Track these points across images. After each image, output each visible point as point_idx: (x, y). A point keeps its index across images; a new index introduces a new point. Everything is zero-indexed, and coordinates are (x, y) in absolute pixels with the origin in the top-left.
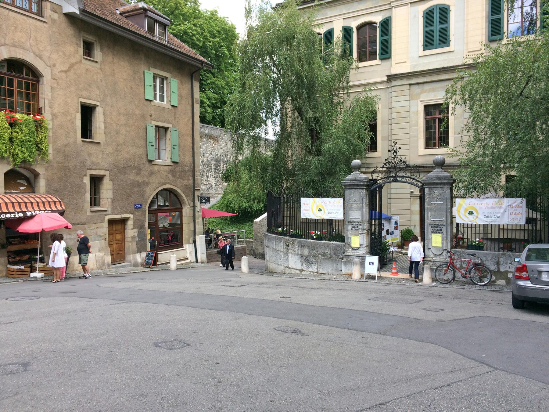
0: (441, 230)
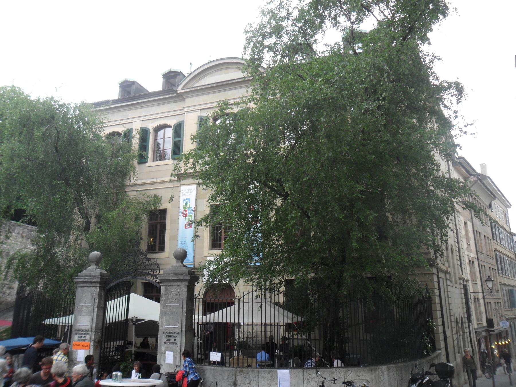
0: (175, 340)
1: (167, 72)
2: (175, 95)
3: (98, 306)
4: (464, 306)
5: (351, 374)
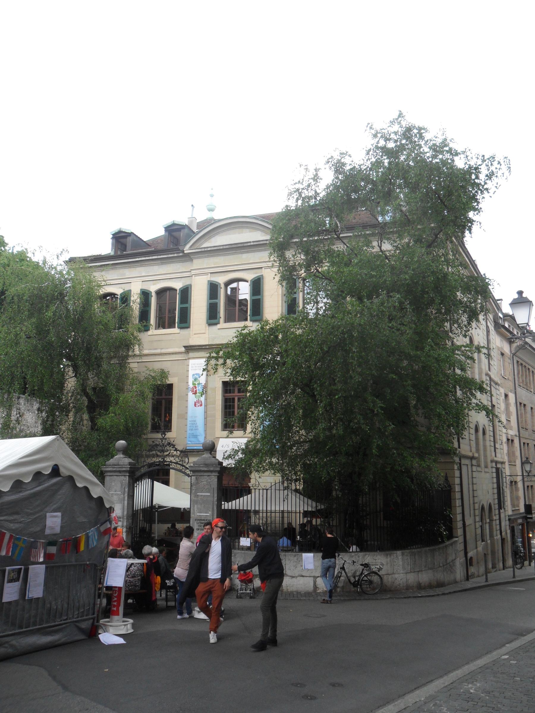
1: (169, 224)
2: (181, 254)
3: (128, 494)
4: (496, 491)
5: (369, 558)
